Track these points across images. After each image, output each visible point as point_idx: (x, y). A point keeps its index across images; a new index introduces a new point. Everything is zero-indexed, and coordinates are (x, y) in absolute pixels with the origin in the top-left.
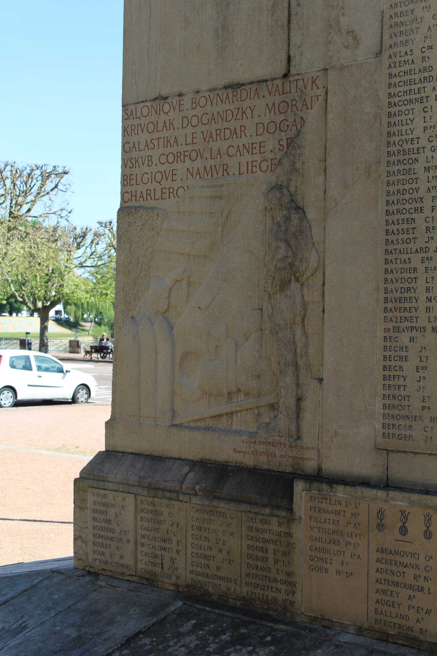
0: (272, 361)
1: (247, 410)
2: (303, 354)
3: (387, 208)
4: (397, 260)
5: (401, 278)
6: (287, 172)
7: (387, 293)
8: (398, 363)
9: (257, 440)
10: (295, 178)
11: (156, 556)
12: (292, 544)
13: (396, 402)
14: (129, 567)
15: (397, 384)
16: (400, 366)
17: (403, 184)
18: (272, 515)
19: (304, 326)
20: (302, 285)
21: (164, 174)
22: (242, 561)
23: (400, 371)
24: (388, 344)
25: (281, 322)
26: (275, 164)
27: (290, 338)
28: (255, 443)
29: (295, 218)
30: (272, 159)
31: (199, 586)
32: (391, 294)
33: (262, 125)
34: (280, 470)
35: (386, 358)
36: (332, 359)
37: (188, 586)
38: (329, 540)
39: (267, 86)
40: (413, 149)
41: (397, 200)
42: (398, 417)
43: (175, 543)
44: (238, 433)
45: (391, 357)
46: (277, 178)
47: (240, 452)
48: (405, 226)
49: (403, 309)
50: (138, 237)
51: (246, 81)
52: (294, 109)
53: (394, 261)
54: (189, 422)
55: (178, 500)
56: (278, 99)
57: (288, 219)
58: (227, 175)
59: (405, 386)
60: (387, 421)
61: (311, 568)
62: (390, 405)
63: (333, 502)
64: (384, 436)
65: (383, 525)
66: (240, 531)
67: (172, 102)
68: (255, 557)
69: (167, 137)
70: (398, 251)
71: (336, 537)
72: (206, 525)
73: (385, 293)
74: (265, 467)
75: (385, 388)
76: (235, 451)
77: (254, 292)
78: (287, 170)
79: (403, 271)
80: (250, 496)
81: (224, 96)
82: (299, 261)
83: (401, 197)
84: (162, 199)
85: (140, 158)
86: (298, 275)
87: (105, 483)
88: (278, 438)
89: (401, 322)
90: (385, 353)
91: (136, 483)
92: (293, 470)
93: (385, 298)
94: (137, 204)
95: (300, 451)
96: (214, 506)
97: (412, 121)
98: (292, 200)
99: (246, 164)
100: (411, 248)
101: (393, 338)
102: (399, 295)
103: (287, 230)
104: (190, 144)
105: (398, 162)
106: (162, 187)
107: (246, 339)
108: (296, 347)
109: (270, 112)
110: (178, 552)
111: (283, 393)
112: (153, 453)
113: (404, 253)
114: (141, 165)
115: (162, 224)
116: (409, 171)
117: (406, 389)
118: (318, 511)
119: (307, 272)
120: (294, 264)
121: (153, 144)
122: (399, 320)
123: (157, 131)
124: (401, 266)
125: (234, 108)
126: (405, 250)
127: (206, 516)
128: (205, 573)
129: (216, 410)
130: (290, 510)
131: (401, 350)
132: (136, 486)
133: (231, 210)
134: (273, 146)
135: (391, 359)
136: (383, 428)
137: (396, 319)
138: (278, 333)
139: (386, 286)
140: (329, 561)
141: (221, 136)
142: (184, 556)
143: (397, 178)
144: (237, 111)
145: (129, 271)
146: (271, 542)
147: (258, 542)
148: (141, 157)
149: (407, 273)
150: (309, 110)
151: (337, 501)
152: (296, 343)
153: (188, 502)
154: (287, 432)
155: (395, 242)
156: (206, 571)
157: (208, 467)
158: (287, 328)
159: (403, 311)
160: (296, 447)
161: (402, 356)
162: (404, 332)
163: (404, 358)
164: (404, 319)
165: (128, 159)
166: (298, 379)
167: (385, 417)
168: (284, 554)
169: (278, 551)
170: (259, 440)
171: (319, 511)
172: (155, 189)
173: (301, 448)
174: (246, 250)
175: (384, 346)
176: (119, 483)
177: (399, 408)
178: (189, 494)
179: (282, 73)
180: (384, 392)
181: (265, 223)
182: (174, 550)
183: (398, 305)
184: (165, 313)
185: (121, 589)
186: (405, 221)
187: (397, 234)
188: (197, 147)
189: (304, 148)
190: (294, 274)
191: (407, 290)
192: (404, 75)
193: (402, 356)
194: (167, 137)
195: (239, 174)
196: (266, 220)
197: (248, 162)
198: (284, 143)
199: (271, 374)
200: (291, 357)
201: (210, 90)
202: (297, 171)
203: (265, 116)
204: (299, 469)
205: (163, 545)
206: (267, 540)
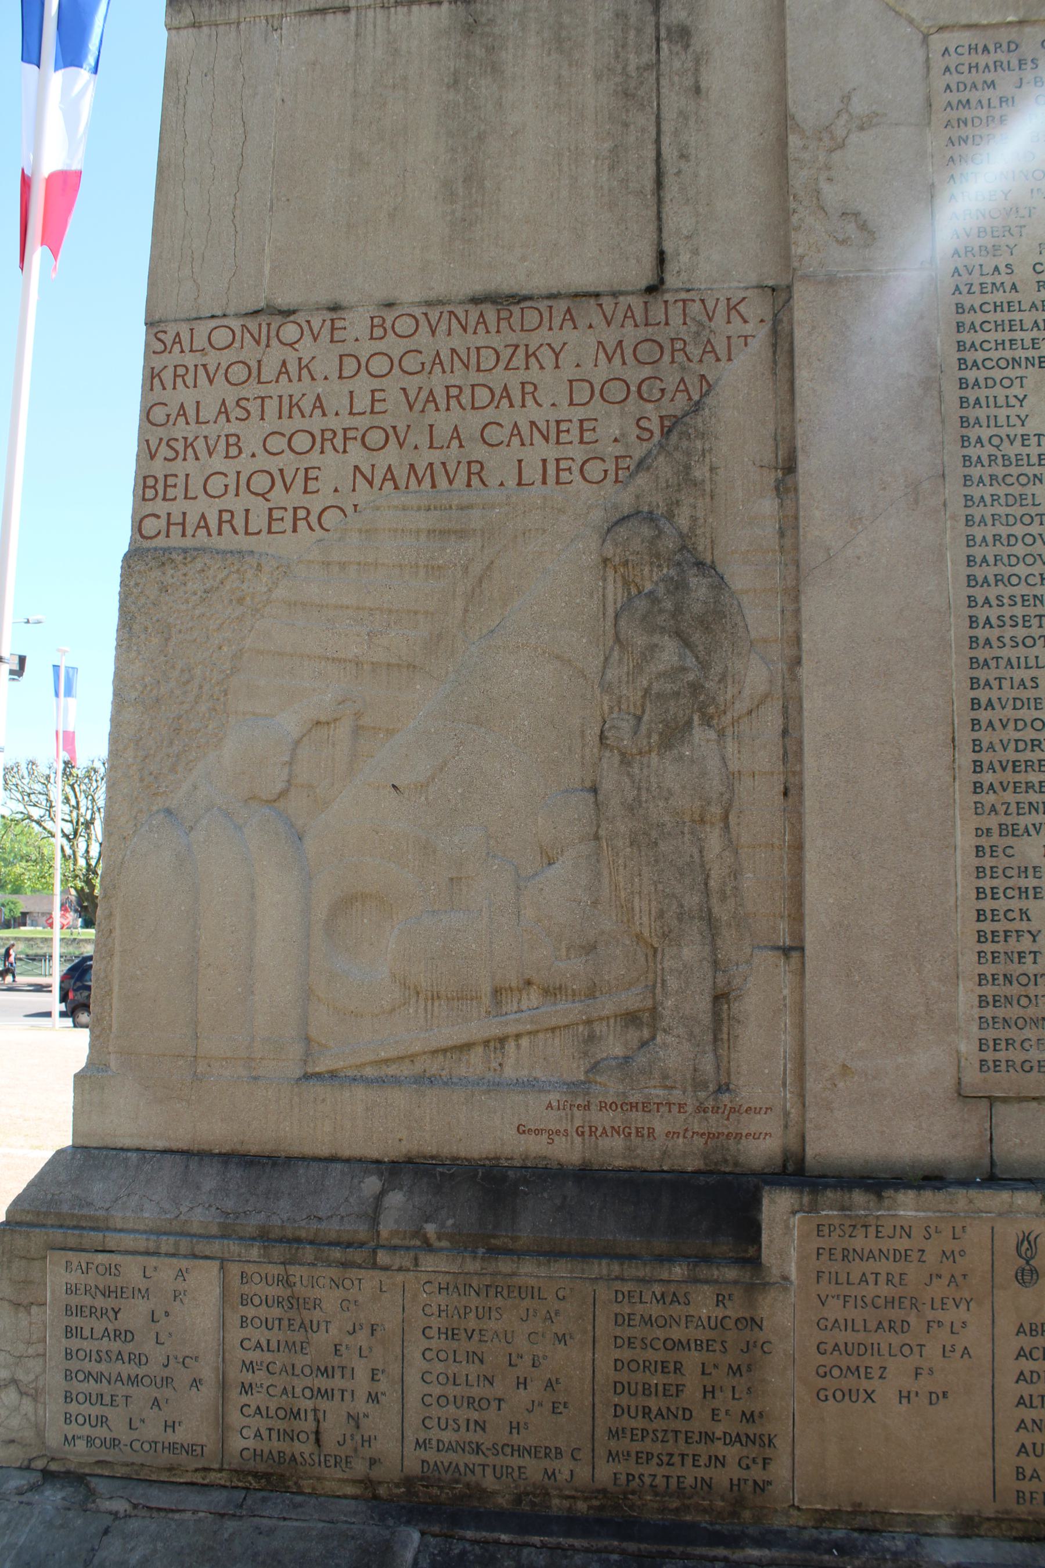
0: (637, 909)
1: (553, 1030)
2: (728, 893)
3: (969, 571)
4: (1003, 681)
5: (1016, 721)
6: (668, 486)
7: (979, 751)
8: (1016, 904)
9: (592, 1101)
10: (692, 500)
11: (296, 1415)
12: (759, 1344)
13: (1014, 990)
14: (199, 1449)
15: (1016, 950)
16: (1021, 910)
17: (1007, 525)
18: (696, 1281)
19: (727, 827)
20: (721, 734)
21: (281, 479)
22: (596, 1401)
23: (1021, 920)
24: (988, 862)
25: (667, 818)
26: (628, 468)
27: (691, 856)
28: (587, 1107)
29: (699, 588)
30: (617, 458)
31: (448, 1476)
32: (991, 754)
33: (587, 385)
34: (665, 1168)
35: (984, 892)
36: (831, 901)
37: (408, 1481)
38: (876, 1323)
39: (600, 305)
40: (1028, 455)
41: (995, 556)
42: (1020, 1023)
43: (362, 1375)
44: (529, 1085)
45: (995, 891)
46: (637, 497)
47: (538, 1132)
48: (1019, 611)
49: (1023, 786)
50: (192, 618)
51: (536, 291)
52: (680, 357)
53: (995, 684)
54: (363, 1065)
55: (375, 1266)
56: (631, 334)
57: (679, 586)
58: (481, 486)
59: (1035, 953)
60: (990, 1034)
61: (820, 1395)
62: (997, 998)
63: (886, 1231)
64: (985, 1068)
65: (1034, 1271)
66: (590, 1327)
67: (308, 322)
68: (640, 1388)
69: (291, 396)
70: (1002, 663)
71: (895, 1314)
72: (472, 1323)
73: (974, 751)
74: (618, 1163)
75: (983, 960)
76: (521, 1130)
77: (570, 750)
78: (667, 481)
79: (1019, 704)
80: (610, 1237)
81: (470, 318)
82: (717, 679)
83: (1004, 550)
84: (270, 532)
85: (201, 440)
86: (711, 710)
87: (107, 1234)
88: (661, 1092)
89: (1018, 814)
90: (981, 883)
91: (214, 1230)
92: (706, 1164)
93: (975, 762)
94: (188, 542)
95: (728, 1119)
96: (500, 1273)
97: (1021, 401)
98: (684, 547)
99: (540, 464)
100: (1037, 657)
101: (1000, 850)
102: (1011, 755)
103: (678, 611)
104: (364, 413)
105: (991, 479)
106: (271, 505)
107: (545, 861)
108: (708, 876)
109: (610, 360)
110: (373, 1398)
111: (673, 983)
112: (241, 1149)
113: (1019, 667)
114: (203, 454)
115: (270, 590)
116: (1021, 499)
117: (1038, 960)
118: (840, 1257)
119: (737, 706)
120: (703, 687)
121: (244, 408)
122: (1013, 808)
123: (259, 382)
124: (1014, 693)
125: (503, 344)
126: (1022, 660)
127: (474, 1301)
128: (471, 1442)
129: (449, 1034)
130: (754, 1263)
131: (1023, 875)
132: (215, 1237)
133: (492, 563)
134: (622, 429)
135: (996, 896)
136: (981, 1050)
137: (1005, 807)
138: (656, 844)
139: (975, 735)
140: (876, 1373)
141: (463, 401)
142: (397, 1407)
143: (993, 510)
144: (510, 350)
145: (158, 700)
146: (693, 1345)
147: (650, 1350)
148: (206, 437)
149: (1029, 708)
150: (722, 363)
151: (898, 1229)
152: (708, 867)
153: (408, 1270)
154: (688, 1076)
155: (995, 643)
156: (477, 1437)
157: (442, 1174)
158: (683, 833)
159: (1023, 789)
160: (716, 1110)
161: (1027, 888)
162: (1029, 835)
163: (1031, 893)
164: (1026, 806)
165: (161, 439)
166: (714, 950)
167: (985, 1025)
168: (736, 1371)
169: (716, 1366)
170: (600, 1099)
171: (844, 1257)
172: (247, 511)
173: (733, 1110)
174: (544, 652)
175: (977, 868)
176: (159, 1233)
177: (1021, 1003)
178: (408, 1248)
179: (643, 284)
180: (982, 969)
181: (604, 596)
182: (362, 1394)
183: (1009, 776)
184: (275, 801)
185: (188, 1515)
186: (1019, 600)
187: (999, 626)
188: (386, 421)
189: (716, 438)
190: (702, 709)
191: (1033, 745)
192: (995, 311)
193: (1027, 888)
194: (291, 396)
195: (519, 484)
196: (604, 588)
197: (544, 461)
198: (655, 426)
199: (628, 942)
200: (696, 899)
201: (429, 304)
202: (696, 485)
203: (596, 365)
204: (726, 1161)
205: (322, 1383)
206: (680, 1341)
